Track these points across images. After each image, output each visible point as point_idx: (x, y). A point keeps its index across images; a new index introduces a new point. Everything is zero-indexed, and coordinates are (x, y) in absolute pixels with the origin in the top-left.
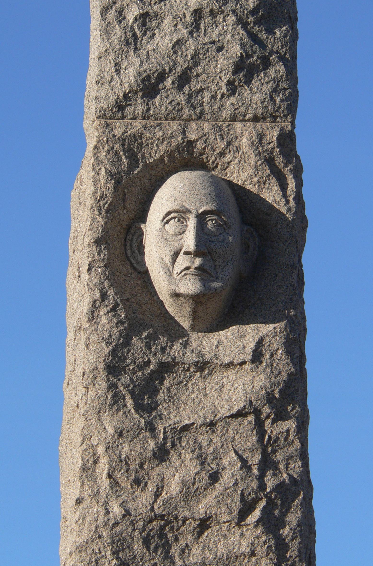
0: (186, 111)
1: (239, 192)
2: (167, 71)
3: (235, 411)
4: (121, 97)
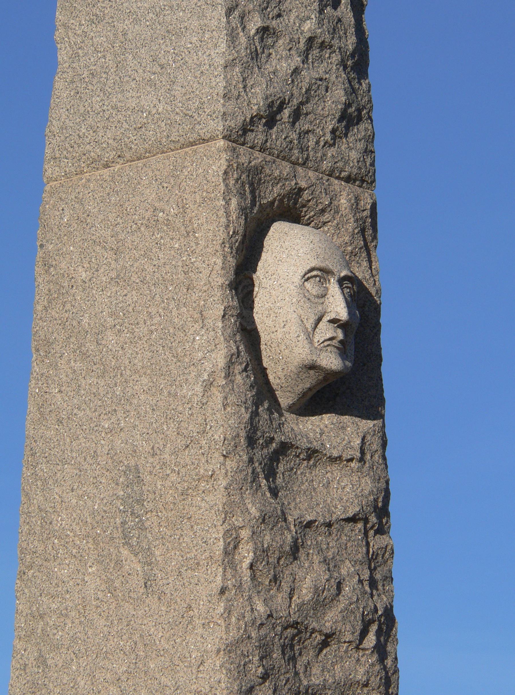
2: (287, 102)
3: (350, 514)
4: (248, 120)
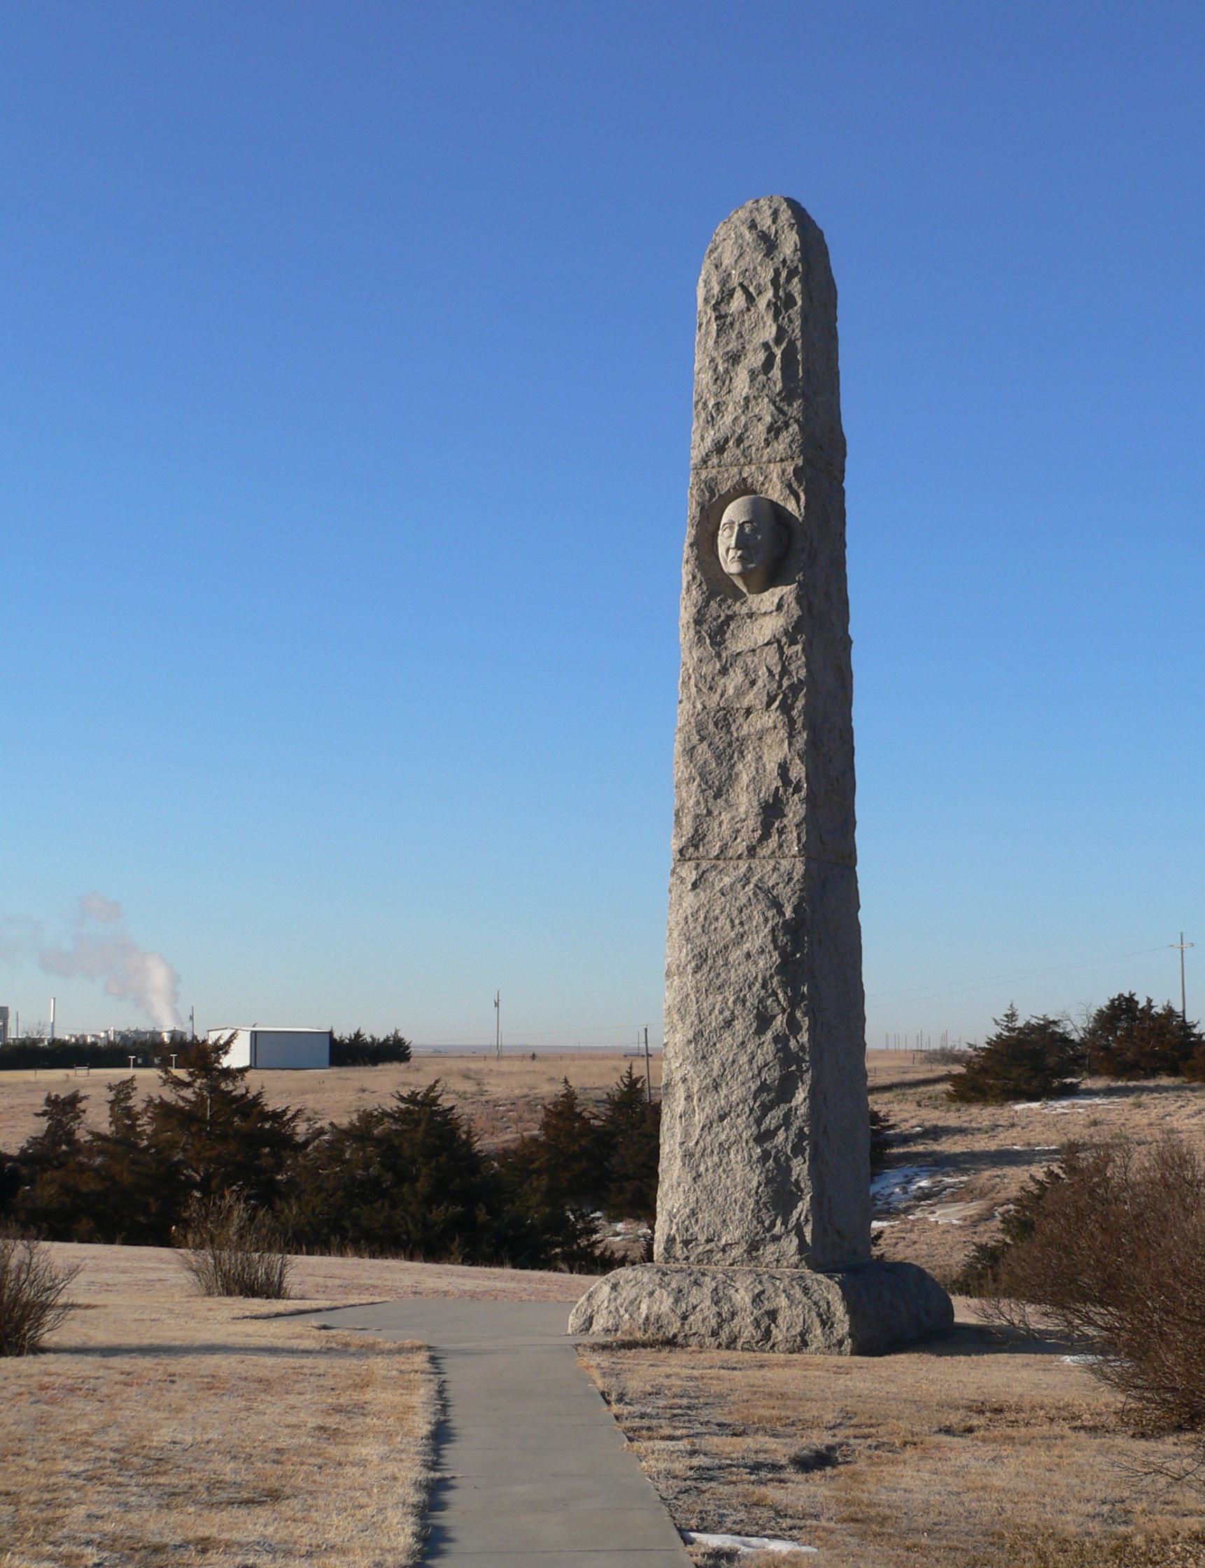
0: (742, 460)
1: (774, 505)
